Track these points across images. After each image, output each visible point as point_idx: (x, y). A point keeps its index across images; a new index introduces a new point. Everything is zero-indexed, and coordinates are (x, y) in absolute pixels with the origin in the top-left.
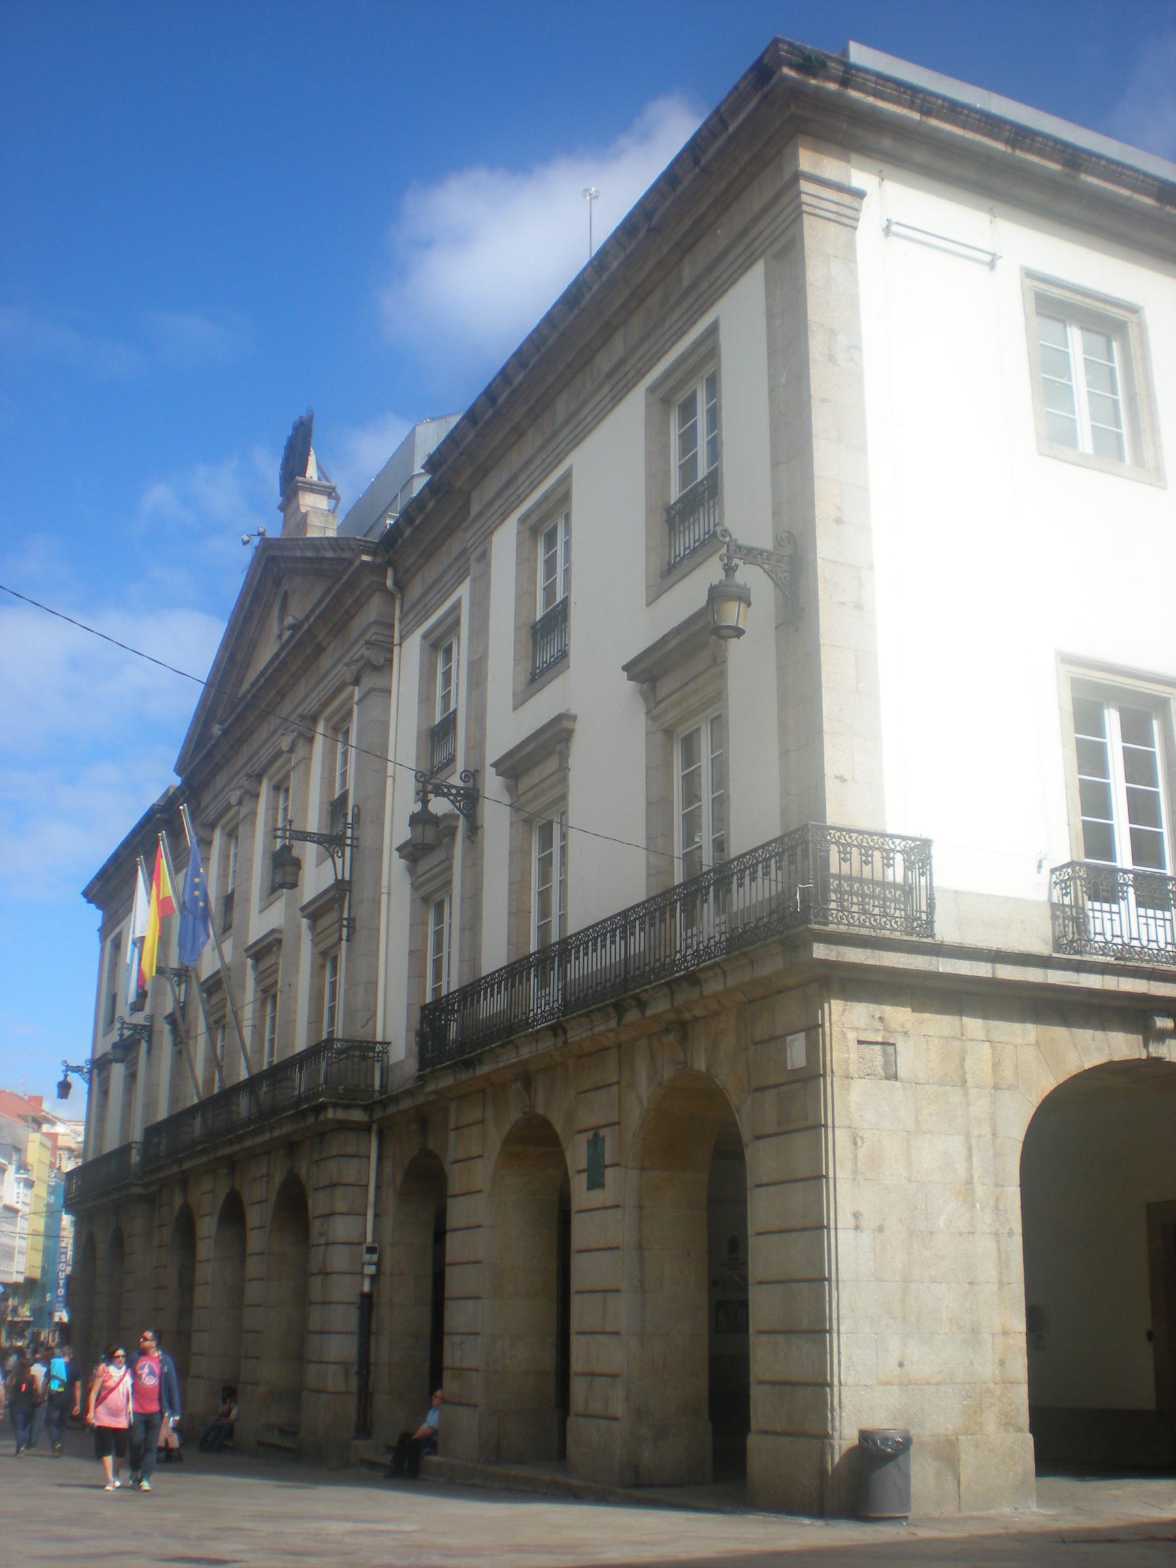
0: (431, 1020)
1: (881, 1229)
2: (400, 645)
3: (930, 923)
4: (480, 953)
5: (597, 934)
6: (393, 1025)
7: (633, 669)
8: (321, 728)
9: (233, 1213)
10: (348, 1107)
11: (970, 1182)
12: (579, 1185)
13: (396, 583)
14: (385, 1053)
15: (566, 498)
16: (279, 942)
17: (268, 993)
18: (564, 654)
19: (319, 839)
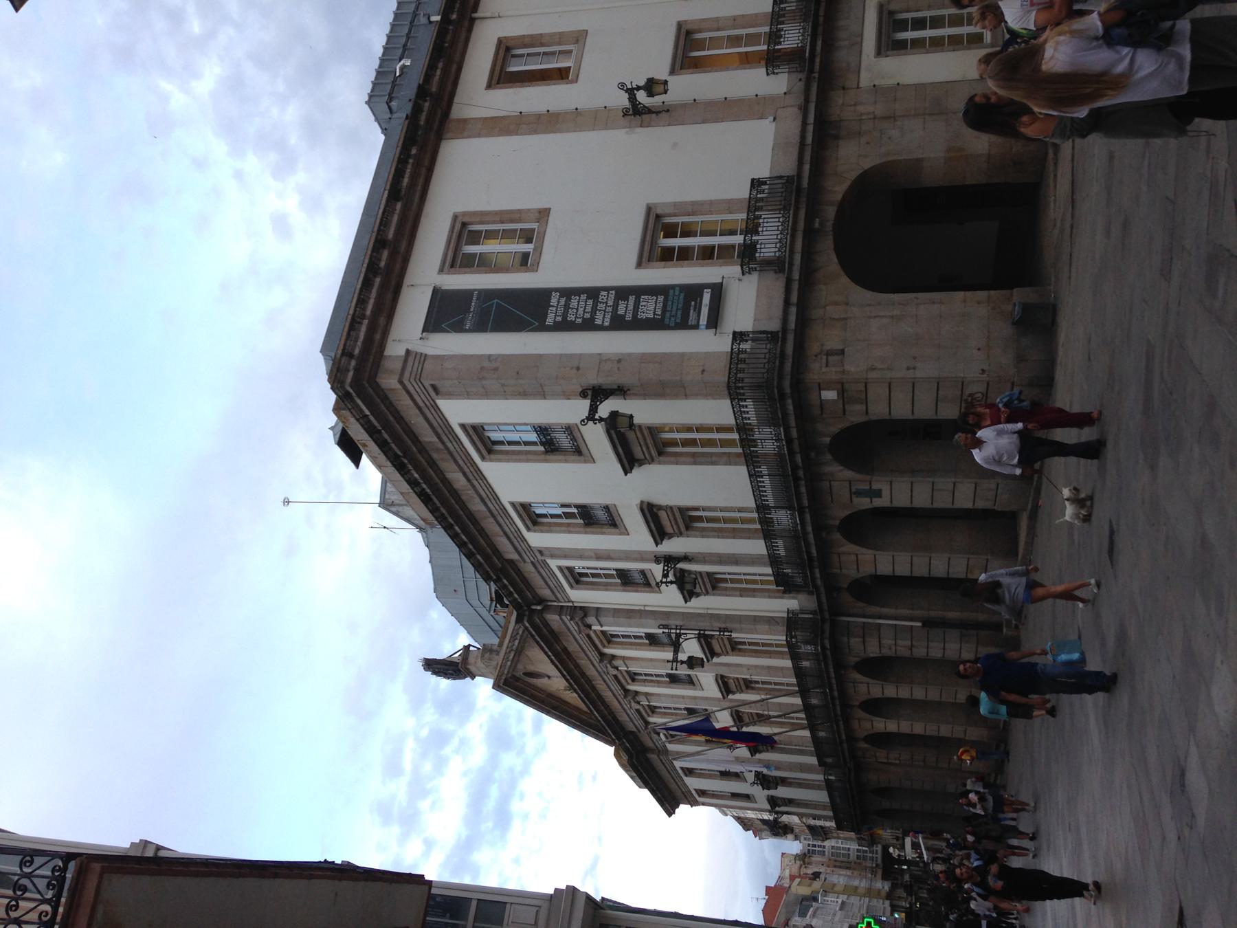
0: (785, 585)
1: (914, 358)
3: (771, 333)
5: (757, 490)
8: (607, 651)
9: (875, 707)
10: (823, 632)
11: (892, 317)
12: (878, 503)
13: (539, 604)
14: (793, 612)
16: (722, 676)
17: (748, 685)
19: (676, 652)
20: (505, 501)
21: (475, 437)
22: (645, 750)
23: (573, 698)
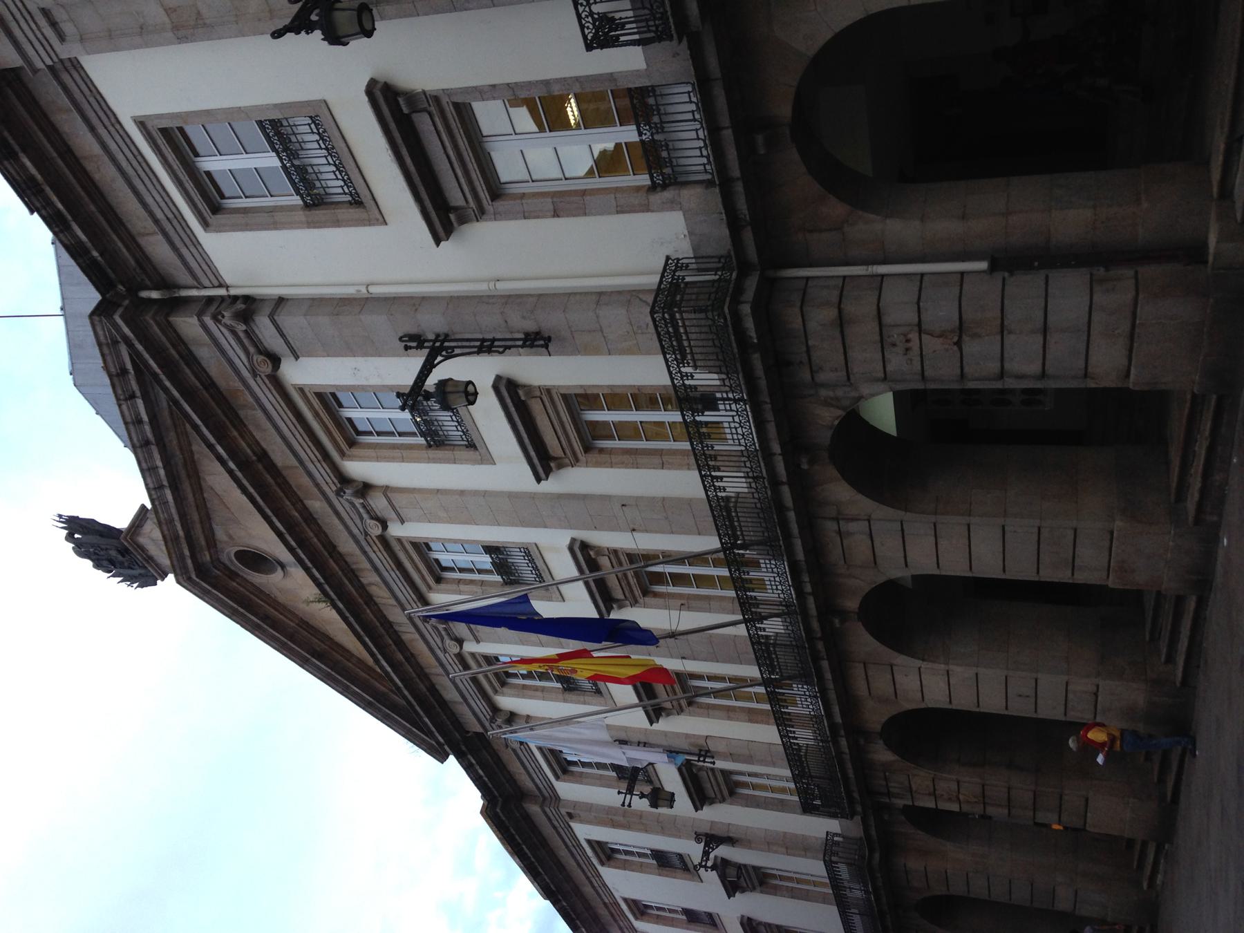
2: (227, 287)
4: (601, 75)
6: (820, 827)
7: (730, 894)
15: (635, 902)
18: (680, 856)
20: (617, 895)
21: (599, 851)
22: (521, 795)
23: (328, 618)
